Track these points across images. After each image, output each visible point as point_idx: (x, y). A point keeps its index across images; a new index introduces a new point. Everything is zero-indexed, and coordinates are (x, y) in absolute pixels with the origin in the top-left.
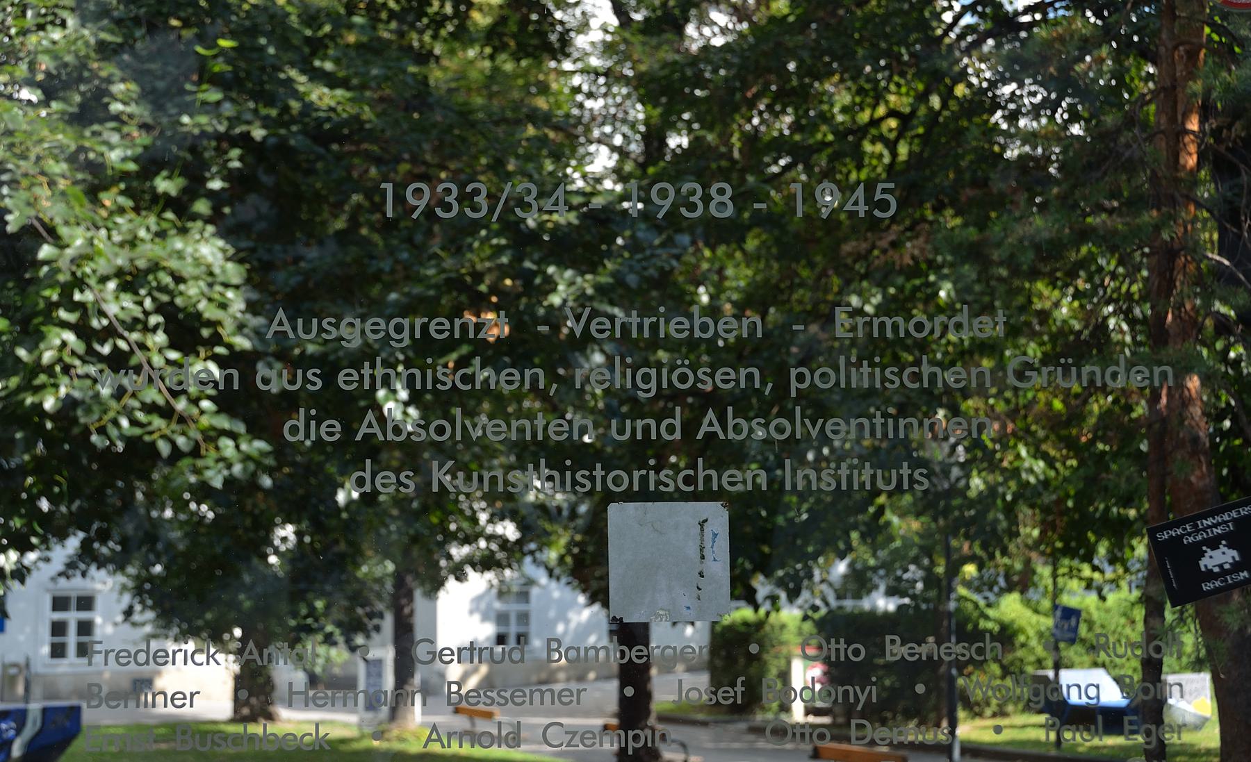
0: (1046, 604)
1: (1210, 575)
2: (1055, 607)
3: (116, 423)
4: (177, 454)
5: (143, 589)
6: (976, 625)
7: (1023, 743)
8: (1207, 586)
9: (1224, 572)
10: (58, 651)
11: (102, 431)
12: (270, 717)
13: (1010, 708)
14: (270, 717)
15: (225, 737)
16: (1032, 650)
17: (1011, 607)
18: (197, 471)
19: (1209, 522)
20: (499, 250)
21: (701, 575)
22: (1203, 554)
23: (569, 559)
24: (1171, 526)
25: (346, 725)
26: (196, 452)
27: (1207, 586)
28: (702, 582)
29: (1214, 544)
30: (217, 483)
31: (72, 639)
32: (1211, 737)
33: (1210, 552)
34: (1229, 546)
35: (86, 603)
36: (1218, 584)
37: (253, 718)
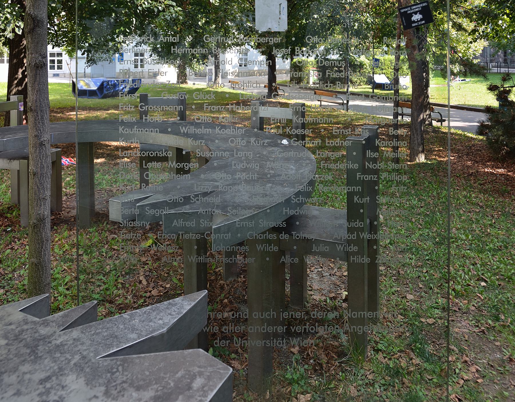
0: (371, 58)
1: (414, 22)
2: (373, 58)
3: (144, 3)
4: (159, 11)
5: (154, 50)
6: (354, 63)
7: (364, 92)
8: (413, 25)
9: (418, 21)
10: (136, 67)
11: (141, 5)
12: (186, 83)
13: (362, 84)
14: (186, 83)
15: (176, 88)
16: (367, 70)
17: (363, 58)
18: (164, 16)
19: (414, 7)
20: (370, 364)
21: (280, 18)
22: (412, 16)
23: (256, 44)
24: (404, 8)
25: (203, 85)
26: (164, 11)
27: (413, 25)
28: (280, 21)
29: (416, 13)
30: (169, 19)
31: (139, 63)
32: (409, 91)
33: (414, 16)
34: (420, 14)
35: (142, 55)
36: (416, 24)
37: (182, 83)
